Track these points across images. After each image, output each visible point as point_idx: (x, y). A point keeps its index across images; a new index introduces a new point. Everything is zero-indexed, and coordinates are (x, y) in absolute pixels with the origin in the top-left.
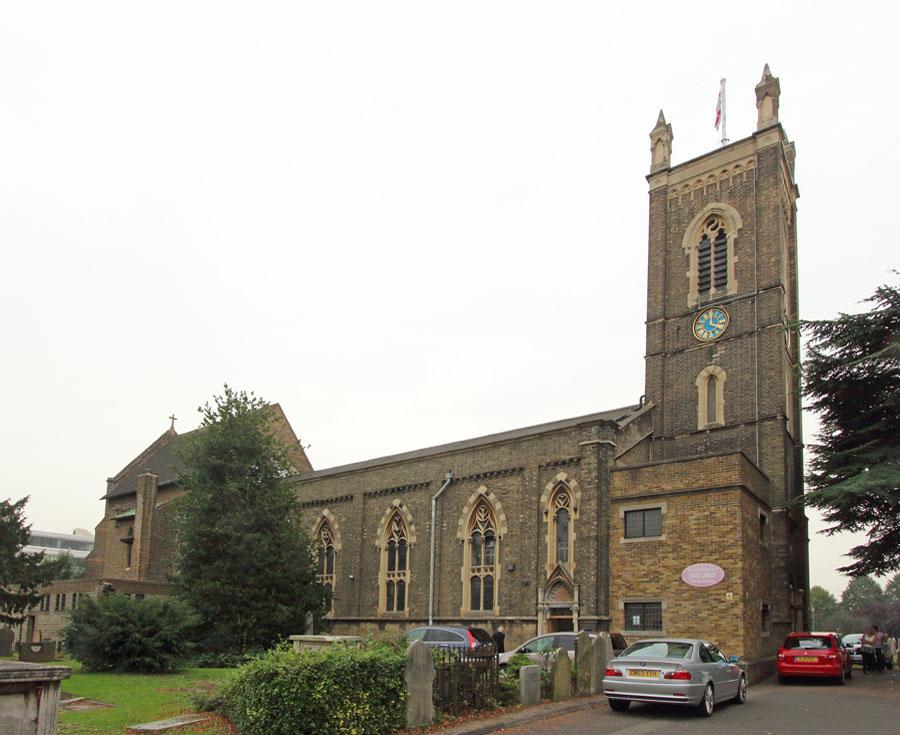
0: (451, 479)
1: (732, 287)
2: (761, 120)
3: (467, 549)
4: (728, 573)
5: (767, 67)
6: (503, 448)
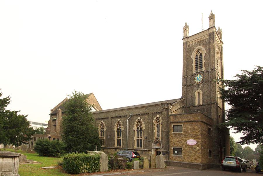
0: (132, 115)
1: (204, 69)
2: (210, 25)
3: (136, 132)
4: (198, 142)
5: (211, 11)
6: (144, 108)
